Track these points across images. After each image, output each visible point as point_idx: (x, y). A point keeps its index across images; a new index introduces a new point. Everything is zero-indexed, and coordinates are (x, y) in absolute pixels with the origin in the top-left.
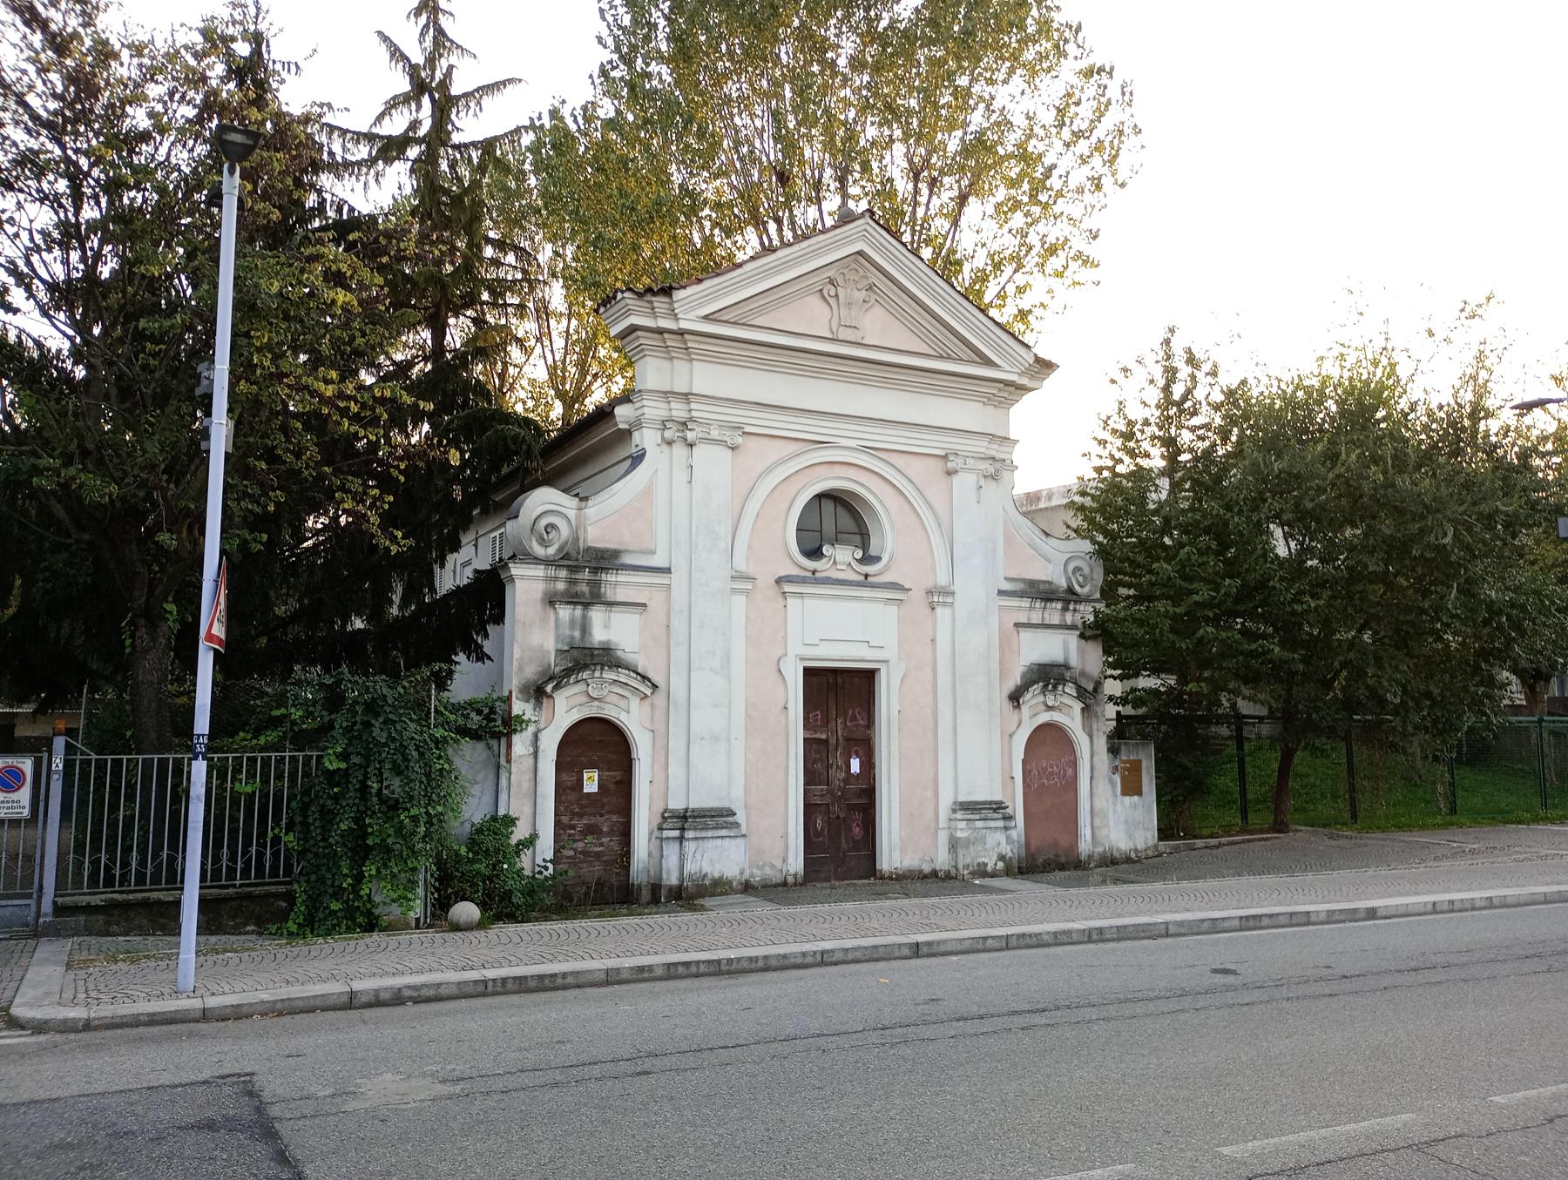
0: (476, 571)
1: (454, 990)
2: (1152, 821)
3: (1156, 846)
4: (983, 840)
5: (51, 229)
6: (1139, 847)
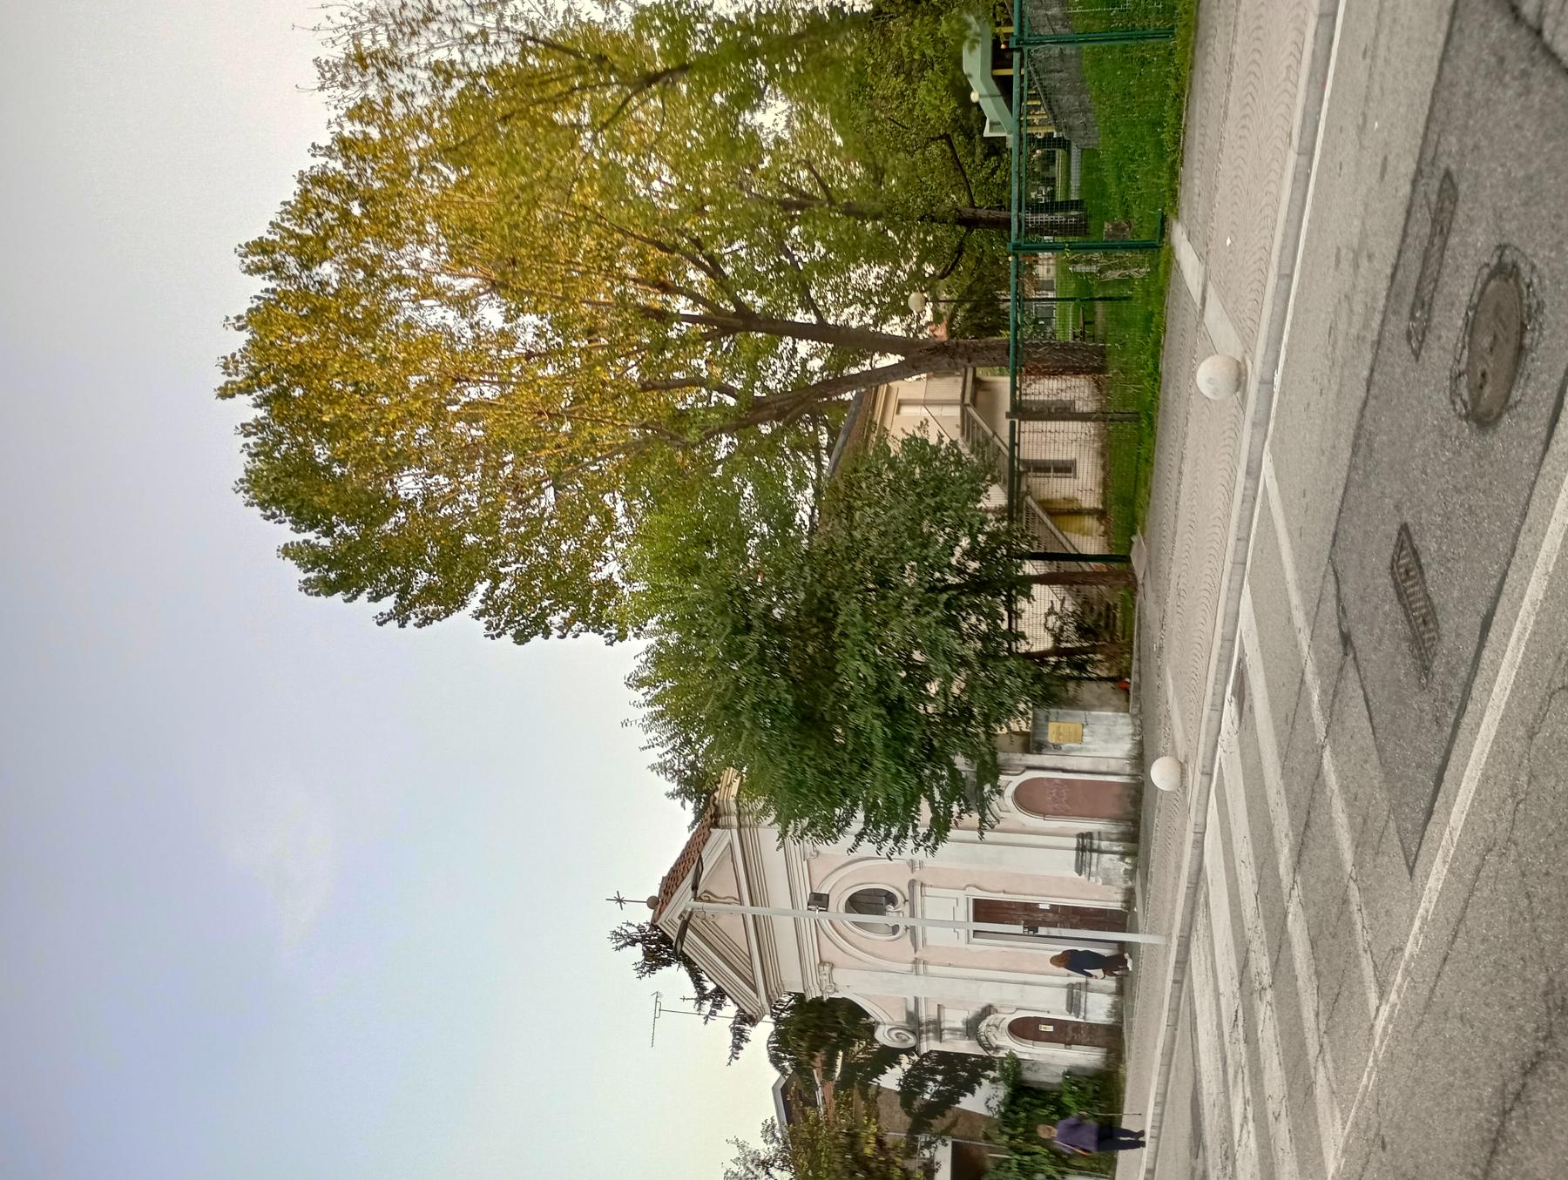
0: (943, 1115)
2: (1107, 717)
3: (1133, 716)
6: (1131, 731)
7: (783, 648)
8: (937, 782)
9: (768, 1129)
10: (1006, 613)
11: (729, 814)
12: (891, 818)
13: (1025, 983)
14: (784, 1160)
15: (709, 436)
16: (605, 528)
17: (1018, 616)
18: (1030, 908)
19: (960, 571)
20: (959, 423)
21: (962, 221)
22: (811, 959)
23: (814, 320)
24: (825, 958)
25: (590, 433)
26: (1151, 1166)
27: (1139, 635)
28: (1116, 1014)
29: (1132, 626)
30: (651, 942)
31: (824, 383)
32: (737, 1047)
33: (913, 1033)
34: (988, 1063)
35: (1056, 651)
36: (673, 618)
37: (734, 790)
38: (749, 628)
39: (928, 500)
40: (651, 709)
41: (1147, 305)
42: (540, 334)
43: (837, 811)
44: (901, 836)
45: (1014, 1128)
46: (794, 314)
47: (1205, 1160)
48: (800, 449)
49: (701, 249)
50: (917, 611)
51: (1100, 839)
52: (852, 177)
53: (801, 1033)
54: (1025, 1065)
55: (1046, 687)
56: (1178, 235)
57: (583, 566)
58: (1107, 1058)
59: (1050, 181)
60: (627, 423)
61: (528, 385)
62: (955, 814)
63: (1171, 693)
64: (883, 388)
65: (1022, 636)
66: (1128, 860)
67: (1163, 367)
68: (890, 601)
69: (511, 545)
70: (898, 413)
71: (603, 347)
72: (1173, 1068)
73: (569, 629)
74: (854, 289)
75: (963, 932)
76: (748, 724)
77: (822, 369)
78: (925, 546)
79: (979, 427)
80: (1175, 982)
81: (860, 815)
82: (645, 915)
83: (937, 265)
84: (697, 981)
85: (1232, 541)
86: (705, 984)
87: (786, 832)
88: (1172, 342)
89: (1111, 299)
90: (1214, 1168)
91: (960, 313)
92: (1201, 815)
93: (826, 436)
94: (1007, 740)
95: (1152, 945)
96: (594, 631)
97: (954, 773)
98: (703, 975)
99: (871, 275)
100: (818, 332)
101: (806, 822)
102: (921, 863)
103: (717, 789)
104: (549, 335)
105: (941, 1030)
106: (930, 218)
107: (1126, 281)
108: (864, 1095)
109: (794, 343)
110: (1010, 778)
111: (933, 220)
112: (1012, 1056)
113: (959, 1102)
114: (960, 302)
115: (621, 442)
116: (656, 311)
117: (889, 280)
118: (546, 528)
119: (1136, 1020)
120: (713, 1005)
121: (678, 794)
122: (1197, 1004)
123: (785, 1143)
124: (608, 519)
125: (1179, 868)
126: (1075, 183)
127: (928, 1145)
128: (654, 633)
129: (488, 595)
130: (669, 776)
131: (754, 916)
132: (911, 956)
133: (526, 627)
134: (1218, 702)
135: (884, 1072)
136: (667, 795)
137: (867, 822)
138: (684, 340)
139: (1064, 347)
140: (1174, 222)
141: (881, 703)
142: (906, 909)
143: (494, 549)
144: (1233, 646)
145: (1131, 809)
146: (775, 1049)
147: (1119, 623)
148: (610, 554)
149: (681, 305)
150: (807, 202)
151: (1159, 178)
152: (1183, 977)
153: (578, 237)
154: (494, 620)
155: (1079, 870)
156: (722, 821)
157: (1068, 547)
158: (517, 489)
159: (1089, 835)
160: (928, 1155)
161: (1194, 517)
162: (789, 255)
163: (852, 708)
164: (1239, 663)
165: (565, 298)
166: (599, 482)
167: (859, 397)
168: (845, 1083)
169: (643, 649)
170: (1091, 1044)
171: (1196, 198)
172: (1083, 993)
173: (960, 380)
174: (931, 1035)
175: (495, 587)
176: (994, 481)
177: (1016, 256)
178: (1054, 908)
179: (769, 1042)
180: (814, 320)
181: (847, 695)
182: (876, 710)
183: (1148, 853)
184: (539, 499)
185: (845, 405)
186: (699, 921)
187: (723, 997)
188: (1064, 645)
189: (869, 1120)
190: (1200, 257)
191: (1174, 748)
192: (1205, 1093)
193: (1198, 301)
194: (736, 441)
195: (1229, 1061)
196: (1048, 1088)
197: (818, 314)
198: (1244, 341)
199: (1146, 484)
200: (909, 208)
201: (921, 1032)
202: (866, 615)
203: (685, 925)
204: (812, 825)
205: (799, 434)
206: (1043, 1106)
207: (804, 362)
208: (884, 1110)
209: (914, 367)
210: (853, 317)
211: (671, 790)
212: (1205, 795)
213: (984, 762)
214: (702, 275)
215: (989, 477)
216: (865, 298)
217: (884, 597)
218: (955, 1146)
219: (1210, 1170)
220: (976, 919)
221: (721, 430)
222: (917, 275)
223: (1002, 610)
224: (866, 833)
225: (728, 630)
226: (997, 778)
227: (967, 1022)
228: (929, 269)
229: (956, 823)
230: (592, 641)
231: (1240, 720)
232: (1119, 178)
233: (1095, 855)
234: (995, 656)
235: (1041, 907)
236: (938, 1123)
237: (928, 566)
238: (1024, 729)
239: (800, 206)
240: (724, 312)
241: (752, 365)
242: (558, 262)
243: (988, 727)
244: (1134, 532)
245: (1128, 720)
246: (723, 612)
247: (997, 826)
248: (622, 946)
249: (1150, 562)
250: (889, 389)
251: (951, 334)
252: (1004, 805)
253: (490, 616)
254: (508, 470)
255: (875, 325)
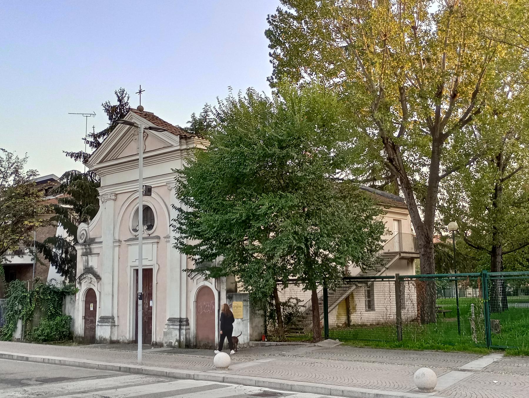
1: (111, 368)
2: (247, 331)
3: (248, 343)
4: (171, 333)
5: (128, 106)
7: (272, 167)
8: (210, 247)
9: (33, 173)
10: (296, 278)
11: (187, 144)
12: (191, 225)
13: (113, 296)
14: (19, 181)
15: (378, 123)
16: (327, 73)
17: (296, 284)
18: (149, 296)
19: (316, 254)
20: (391, 251)
21: (494, 249)
22: (119, 189)
23: (440, 175)
24: (119, 196)
25: (376, 62)
26: (30, 359)
27: (289, 345)
28: (101, 340)
29: (294, 341)
30: (120, 109)
31: (408, 181)
32: (72, 155)
33: (85, 242)
34: (72, 279)
35: (278, 304)
36: (284, 110)
37: (199, 146)
38: (282, 148)
39: (351, 236)
40: (237, 101)
41: (458, 343)
42: (426, 33)
43: (192, 198)
44: (182, 230)
45: (43, 293)
46: (443, 164)
47: (36, 385)
48: (373, 171)
49: (475, 114)
50: (296, 233)
51: (186, 329)
52: (515, 191)
53: (80, 186)
54: (73, 297)
55: (260, 300)
56: (497, 357)
57: (308, 63)
58: (79, 337)
59: (516, 293)
60: (383, 81)
61: (400, 28)
62: (194, 257)
63: (262, 361)
64: (407, 212)
65: (286, 286)
66: (177, 343)
67: (427, 352)
68: (299, 219)
69: (316, 25)
70: (394, 220)
71: (421, 66)
72: (78, 368)
73: (274, 58)
74: (456, 195)
75: (137, 263)
76: (233, 150)
77: (415, 180)
78: (328, 236)
79: (389, 261)
80: (120, 368)
81: (191, 210)
82: (133, 104)
83: (471, 237)
84: (103, 134)
85: (342, 388)
86: (102, 138)
87: (181, 173)
88: (440, 356)
89: (459, 324)
90: (32, 389)
91: (446, 250)
92: (203, 378)
93: (380, 184)
94: (233, 281)
95: (137, 356)
96: (274, 71)
97: (215, 255)
98: (106, 136)
99: (465, 204)
100: (434, 178)
101: (186, 183)
102: (169, 241)
103: (199, 138)
104: (426, 38)
105: (87, 255)
106: (495, 232)
107: (469, 331)
108: (52, 219)
109: (428, 165)
110: (214, 283)
111: (494, 234)
112: (77, 290)
113: (53, 265)
114: (454, 250)
115: (373, 78)
116: (441, 93)
117: (462, 212)
118: (326, 43)
119: (99, 350)
120: (91, 142)
121: (194, 119)
122: (110, 379)
123: (27, 181)
124: (332, 74)
125: (176, 367)
126: (516, 305)
127: (31, 252)
128: (276, 102)
129: (290, 15)
130: (203, 114)
131: (138, 159)
132: (123, 239)
133: (274, 36)
134: (260, 384)
135: (64, 228)
136: (194, 114)
137: (188, 213)
138: (426, 108)
139: (433, 302)
140: (502, 355)
141: (248, 218)
142: (146, 235)
143: (313, 16)
144: (289, 390)
145: (202, 344)
146: (72, 174)
147: (293, 335)
148: (314, 77)
149: (445, 106)
150: (502, 168)
151: (525, 346)
152: (122, 371)
153: (478, 49)
154: (277, 19)
155: (170, 320)
156: (183, 141)
157: (331, 308)
158: (345, 27)
159: (188, 324)
160: (26, 251)
161: (352, 369)
162: (474, 159)
163: (244, 202)
164: (280, 393)
165: (446, 45)
166: (352, 68)
167: (401, 200)
168: (58, 210)
169: (268, 95)
170: (86, 329)
171: (516, 365)
172: (110, 324)
173: (413, 251)
174: (85, 250)
175: (294, 18)
176: (363, 269)
177: (481, 276)
178: (150, 308)
179: (75, 171)
180: (440, 175)
181: (250, 200)
182: (244, 214)
183: (181, 353)
184: (341, 38)
185: (397, 193)
186: (133, 132)
187: (96, 146)
188: (282, 307)
189: (41, 222)
190: (486, 368)
191: (235, 363)
192: (68, 383)
193: (463, 367)
194: (376, 138)
195: (84, 395)
196: (63, 309)
197: (443, 176)
198: (445, 391)
199: (366, 345)
200: (500, 221)
201: (85, 246)
202: (291, 208)
203: (132, 124)
204: (185, 186)
205: (380, 170)
206: (54, 308)
207: (418, 171)
208: (46, 229)
209: (418, 227)
210: (442, 195)
211: (196, 116)
212: (213, 379)
213: (221, 270)
214: (460, 116)
215: (365, 267)
216: (452, 201)
217: (301, 216)
218: (31, 265)
219: (31, 387)
220: (143, 270)
221: (381, 130)
222: (464, 227)
223: (298, 275)
224: (182, 213)
225: (280, 138)
226: (213, 277)
227: (92, 268)
228: (469, 233)
229: (190, 258)
230: (269, 70)
231: (252, 395)
232: (523, 326)
233: (178, 327)
234: (274, 274)
235: (151, 302)
236: (42, 256)
237: (318, 237)
238: (238, 290)
239: (499, 164)
240: (442, 128)
241: (416, 144)
242: (464, 40)
243: (239, 271)
244: (340, 340)
245: (246, 341)
246: (289, 135)
247: (189, 278)
248: (117, 95)
249: (327, 349)
250: (407, 215)
251: (436, 245)
252: (200, 281)
253: (279, 17)
254: (354, 21)
255: (439, 206)
